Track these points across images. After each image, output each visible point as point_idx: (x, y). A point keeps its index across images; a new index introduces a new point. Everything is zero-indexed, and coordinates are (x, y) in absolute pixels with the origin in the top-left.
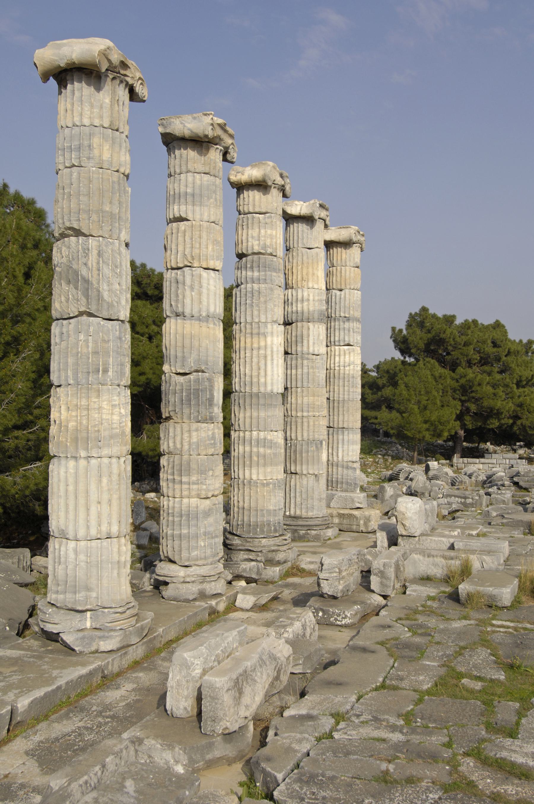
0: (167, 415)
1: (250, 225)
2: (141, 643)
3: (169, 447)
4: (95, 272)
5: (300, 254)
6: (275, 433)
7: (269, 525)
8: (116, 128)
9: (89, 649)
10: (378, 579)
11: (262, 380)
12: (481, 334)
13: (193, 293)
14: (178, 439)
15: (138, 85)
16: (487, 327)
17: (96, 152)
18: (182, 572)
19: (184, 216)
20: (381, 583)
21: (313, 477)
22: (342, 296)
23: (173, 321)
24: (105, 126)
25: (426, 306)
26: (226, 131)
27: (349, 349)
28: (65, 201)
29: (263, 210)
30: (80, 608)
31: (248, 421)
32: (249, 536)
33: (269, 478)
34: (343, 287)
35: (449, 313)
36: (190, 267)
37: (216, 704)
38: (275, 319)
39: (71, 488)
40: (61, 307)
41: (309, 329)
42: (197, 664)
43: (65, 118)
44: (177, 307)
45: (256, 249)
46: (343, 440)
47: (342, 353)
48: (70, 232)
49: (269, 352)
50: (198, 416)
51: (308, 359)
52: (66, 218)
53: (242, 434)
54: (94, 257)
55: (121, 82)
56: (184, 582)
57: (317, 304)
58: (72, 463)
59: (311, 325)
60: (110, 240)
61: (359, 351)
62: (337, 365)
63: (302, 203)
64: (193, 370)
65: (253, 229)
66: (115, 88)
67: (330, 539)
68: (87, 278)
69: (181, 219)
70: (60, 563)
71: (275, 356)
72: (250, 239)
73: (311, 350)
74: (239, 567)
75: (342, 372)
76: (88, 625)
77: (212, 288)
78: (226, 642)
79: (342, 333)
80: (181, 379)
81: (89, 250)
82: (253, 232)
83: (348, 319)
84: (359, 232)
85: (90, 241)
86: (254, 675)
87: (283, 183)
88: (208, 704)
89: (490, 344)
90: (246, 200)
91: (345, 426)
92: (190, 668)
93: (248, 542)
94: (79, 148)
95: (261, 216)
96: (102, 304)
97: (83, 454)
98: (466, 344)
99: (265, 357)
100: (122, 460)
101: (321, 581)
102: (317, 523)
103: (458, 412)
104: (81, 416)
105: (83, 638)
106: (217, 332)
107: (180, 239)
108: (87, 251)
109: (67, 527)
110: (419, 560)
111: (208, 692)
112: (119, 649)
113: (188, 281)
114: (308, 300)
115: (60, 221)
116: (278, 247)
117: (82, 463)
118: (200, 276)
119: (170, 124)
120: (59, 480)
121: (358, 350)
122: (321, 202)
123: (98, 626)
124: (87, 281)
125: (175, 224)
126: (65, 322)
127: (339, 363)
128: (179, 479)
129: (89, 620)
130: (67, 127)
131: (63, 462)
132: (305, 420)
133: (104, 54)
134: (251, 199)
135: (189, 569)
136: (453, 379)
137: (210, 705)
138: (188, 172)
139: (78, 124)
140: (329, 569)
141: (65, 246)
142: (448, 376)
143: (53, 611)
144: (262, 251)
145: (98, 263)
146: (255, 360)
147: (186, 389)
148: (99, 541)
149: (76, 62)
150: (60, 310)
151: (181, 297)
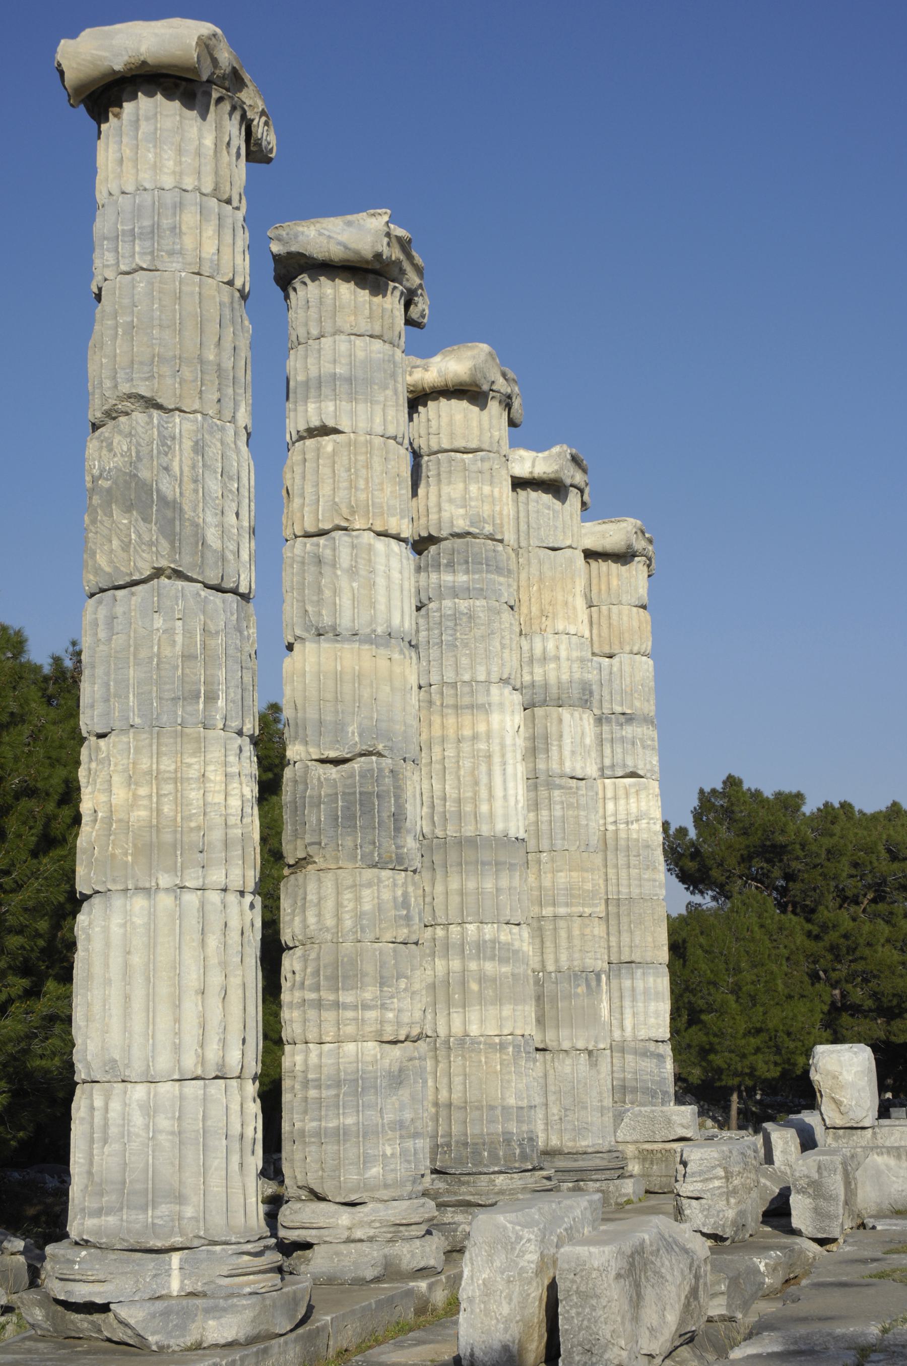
0: (301, 854)
1: (444, 476)
2: (293, 1335)
3: (305, 927)
4: (189, 486)
5: (534, 561)
6: (516, 929)
7: (508, 1142)
8: (225, 197)
9: (181, 1341)
10: (808, 1201)
11: (484, 808)
12: (862, 833)
13: (355, 585)
14: (329, 904)
15: (261, 124)
16: (875, 817)
17: (189, 242)
18: (345, 1217)
19: (331, 423)
20: (816, 1210)
21: (584, 1056)
22: (615, 669)
23: (310, 646)
24: (204, 191)
25: (736, 774)
26: (410, 257)
27: (635, 785)
28: (118, 341)
29: (473, 445)
30: (159, 1244)
31: (455, 900)
32: (465, 1170)
33: (506, 1032)
34: (616, 649)
35: (789, 788)
36: (345, 529)
37: (593, 1308)
38: (505, 676)
39: (137, 960)
40: (111, 562)
41: (560, 721)
42: (529, 1240)
43: (119, 176)
44: (320, 614)
45: (461, 525)
46: (633, 989)
47: (621, 793)
48: (128, 405)
49: (496, 748)
50: (372, 853)
51: (561, 787)
52: (121, 375)
53: (440, 932)
54: (186, 454)
55: (234, 108)
56: (349, 1241)
57: (575, 666)
58: (139, 903)
59: (565, 713)
60: (218, 422)
61: (657, 791)
62: (610, 819)
63: (534, 454)
64: (357, 750)
65: (450, 483)
66: (221, 119)
67: (629, 1202)
68: (170, 498)
69: (325, 431)
70: (105, 1141)
71: (509, 756)
72: (445, 506)
73: (568, 768)
74: (455, 1230)
75: (622, 835)
76: (175, 1286)
77: (396, 575)
78: (571, 1216)
79: (619, 750)
80: (333, 772)
81: (174, 438)
82: (455, 489)
83: (629, 718)
84: (643, 533)
85: (177, 420)
86: (658, 1264)
87: (509, 391)
88: (573, 1312)
89: (884, 854)
90: (434, 423)
91: (636, 957)
92: (513, 1249)
93: (464, 1183)
94: (154, 232)
95: (465, 456)
96: (202, 553)
97: (165, 880)
98: (830, 853)
99: (489, 757)
100: (249, 898)
101: (685, 1202)
102: (597, 1162)
103: (826, 1008)
104: (159, 796)
105: (166, 1313)
106: (407, 672)
107: (325, 471)
108: (166, 441)
109: (127, 1049)
110: (889, 1168)
111: (573, 1281)
112: (251, 1341)
113: (345, 559)
114: (557, 658)
115: (108, 383)
116: (506, 520)
117: (165, 901)
118: (370, 548)
119: (296, 236)
120: (107, 945)
121: (655, 786)
122: (574, 451)
123: (199, 1287)
124: (172, 506)
125: (310, 443)
126: (120, 593)
127: (616, 814)
128: (332, 997)
129: (176, 1274)
130: (123, 193)
131: (117, 902)
132: (562, 924)
133: (207, 46)
134: (444, 420)
135: (359, 1208)
136: (809, 934)
137: (578, 1314)
138: (338, 332)
139: (148, 186)
140: (701, 1173)
141: (120, 432)
142: (798, 927)
143: (89, 1254)
144: (472, 530)
145: (194, 467)
146: (466, 764)
147: (344, 793)
148: (201, 1082)
149: (149, 61)
150: (107, 569)
151: (327, 593)
